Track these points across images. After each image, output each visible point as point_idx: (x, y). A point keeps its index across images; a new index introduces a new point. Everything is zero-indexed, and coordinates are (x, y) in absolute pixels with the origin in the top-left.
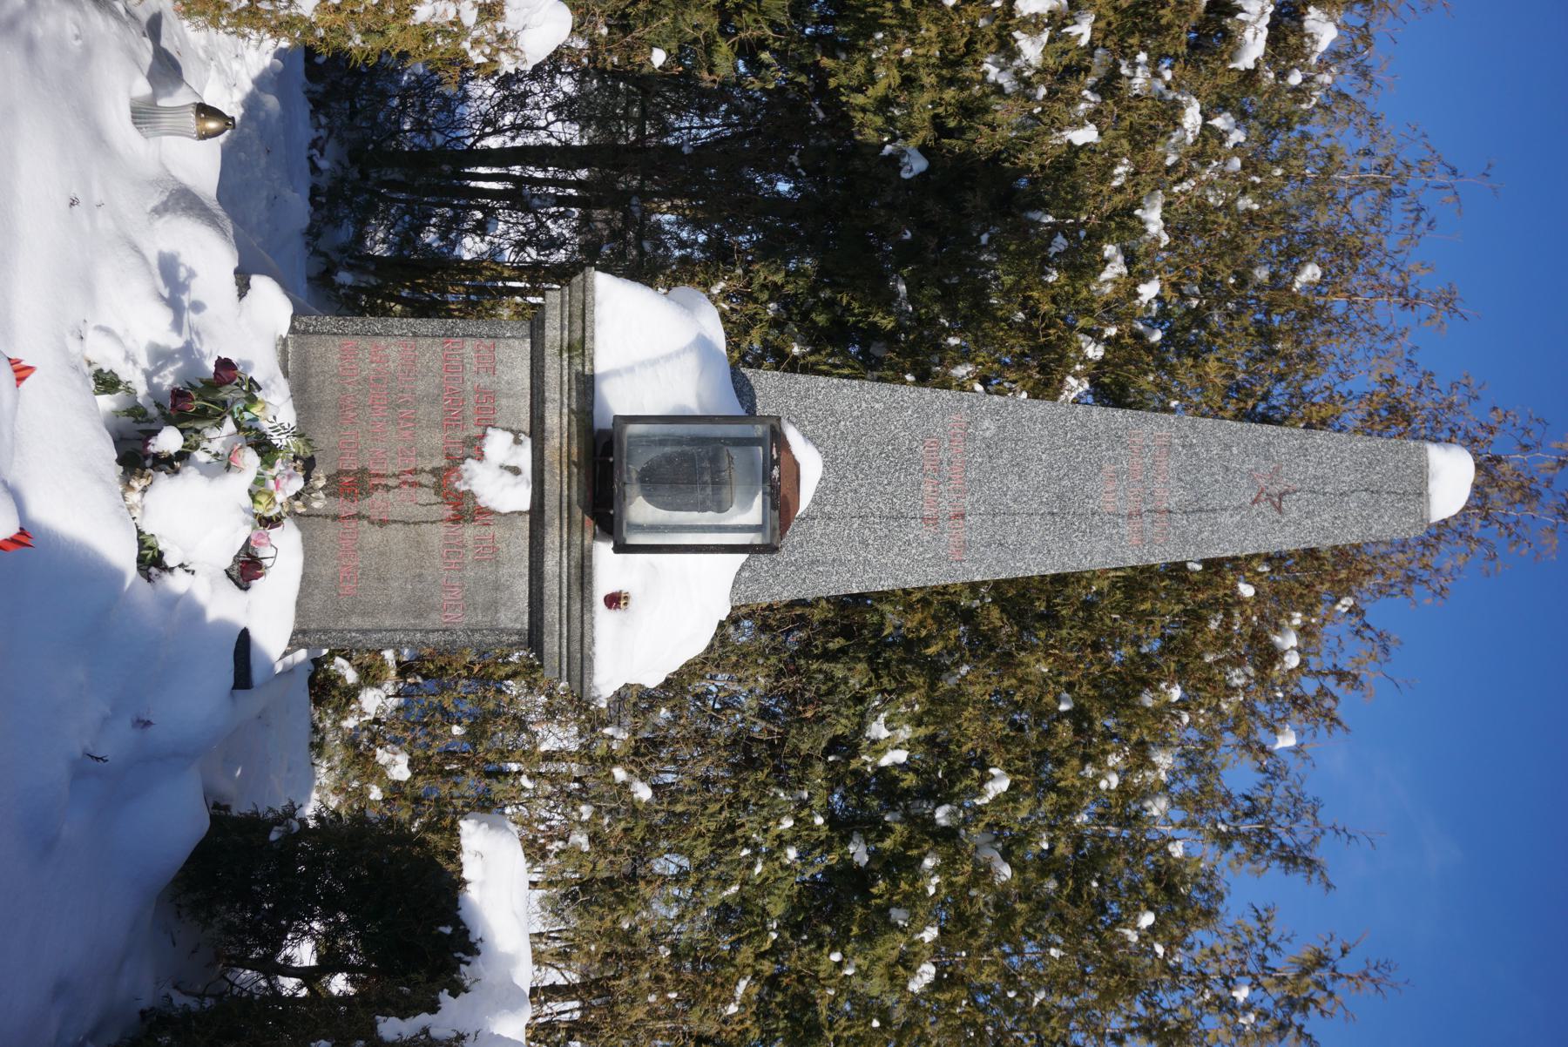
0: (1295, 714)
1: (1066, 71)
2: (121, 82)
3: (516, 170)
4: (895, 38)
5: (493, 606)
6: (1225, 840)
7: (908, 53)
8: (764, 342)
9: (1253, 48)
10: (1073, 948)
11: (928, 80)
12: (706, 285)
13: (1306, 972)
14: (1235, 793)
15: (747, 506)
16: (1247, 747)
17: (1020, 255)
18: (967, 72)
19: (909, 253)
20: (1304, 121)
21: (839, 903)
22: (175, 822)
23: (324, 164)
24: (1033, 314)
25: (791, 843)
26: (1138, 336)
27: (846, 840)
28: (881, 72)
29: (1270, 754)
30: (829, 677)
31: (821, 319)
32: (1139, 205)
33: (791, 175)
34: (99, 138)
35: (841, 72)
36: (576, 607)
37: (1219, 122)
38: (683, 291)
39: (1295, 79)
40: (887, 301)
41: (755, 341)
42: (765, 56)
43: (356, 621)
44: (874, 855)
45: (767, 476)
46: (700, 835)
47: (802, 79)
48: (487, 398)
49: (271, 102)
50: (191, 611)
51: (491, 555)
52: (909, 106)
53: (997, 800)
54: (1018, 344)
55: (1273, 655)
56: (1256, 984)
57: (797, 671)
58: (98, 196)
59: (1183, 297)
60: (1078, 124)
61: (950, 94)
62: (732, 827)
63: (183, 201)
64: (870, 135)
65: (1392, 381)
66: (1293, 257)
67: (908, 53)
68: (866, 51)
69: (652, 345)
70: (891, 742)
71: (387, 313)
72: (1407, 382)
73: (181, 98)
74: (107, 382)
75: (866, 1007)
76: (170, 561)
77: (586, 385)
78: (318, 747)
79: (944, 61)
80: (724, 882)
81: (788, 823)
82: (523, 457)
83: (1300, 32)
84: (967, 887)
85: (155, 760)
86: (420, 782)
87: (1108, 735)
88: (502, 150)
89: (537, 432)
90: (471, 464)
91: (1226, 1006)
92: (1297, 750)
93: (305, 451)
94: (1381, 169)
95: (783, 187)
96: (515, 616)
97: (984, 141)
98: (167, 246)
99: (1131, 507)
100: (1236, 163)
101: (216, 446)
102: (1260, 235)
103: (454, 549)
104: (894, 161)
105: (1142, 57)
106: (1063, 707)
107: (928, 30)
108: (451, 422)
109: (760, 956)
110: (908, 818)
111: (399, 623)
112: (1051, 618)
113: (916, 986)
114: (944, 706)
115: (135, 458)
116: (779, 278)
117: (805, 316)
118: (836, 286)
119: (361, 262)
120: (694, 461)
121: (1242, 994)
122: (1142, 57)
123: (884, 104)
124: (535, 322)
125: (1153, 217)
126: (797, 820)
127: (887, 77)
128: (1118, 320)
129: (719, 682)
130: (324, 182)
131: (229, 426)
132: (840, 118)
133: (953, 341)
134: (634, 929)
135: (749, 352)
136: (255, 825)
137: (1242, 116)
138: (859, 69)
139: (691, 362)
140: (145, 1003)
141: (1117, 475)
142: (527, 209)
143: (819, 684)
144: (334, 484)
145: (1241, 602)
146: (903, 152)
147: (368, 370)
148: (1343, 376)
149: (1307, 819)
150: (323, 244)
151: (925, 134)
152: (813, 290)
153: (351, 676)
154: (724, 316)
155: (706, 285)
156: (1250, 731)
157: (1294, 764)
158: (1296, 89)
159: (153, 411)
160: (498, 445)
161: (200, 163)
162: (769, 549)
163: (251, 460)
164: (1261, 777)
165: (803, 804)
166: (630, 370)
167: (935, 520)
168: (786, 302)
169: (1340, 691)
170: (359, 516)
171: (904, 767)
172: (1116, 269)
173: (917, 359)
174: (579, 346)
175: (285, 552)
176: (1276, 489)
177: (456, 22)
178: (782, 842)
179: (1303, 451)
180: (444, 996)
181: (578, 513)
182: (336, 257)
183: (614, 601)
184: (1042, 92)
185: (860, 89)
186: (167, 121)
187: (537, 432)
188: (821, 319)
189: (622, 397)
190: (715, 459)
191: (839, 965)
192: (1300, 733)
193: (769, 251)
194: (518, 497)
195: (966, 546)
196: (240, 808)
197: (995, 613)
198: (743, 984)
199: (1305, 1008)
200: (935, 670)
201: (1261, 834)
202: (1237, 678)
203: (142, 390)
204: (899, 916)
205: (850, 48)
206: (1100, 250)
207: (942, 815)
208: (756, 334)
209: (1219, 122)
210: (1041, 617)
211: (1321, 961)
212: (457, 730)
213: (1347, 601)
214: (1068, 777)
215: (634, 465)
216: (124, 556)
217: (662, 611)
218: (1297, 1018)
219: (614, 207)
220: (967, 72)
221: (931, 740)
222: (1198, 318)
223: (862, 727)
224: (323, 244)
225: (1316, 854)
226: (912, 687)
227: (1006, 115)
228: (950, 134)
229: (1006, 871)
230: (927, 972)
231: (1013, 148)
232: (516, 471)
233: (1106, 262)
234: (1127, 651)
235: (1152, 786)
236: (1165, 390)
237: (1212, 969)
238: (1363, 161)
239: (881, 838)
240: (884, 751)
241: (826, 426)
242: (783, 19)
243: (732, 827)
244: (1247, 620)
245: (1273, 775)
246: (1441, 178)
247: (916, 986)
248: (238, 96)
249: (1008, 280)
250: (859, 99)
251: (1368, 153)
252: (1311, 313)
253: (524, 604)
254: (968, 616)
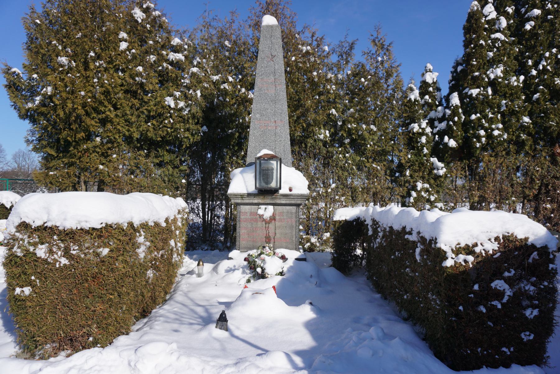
0: (321, 46)
1: (186, 97)
2: (194, 279)
3: (207, 210)
4: (179, 132)
5: (291, 213)
6: (347, 62)
7: (182, 130)
8: (241, 160)
9: (180, 56)
10: (369, 95)
11: (188, 126)
12: (230, 172)
13: (376, 45)
14: (337, 59)
15: (273, 164)
16: (327, 57)
17: (223, 107)
18: (186, 118)
19: (223, 130)
20: (195, 45)
21: (358, 145)
22: (332, 273)
23: (206, 248)
24: (235, 103)
25: (345, 155)
26: (240, 81)
27: (344, 144)
28: (186, 135)
29: (329, 52)
30: (310, 147)
31: (236, 148)
32: (213, 81)
33: (206, 154)
34: (205, 282)
35: (186, 144)
36: (292, 197)
37: (195, 63)
38: (231, 176)
39: (186, 47)
40: (233, 134)
41: (241, 162)
42: (183, 159)
43: (294, 239)
44: (347, 137)
45: (267, 160)
46: (343, 174)
47: (188, 152)
48: (251, 214)
49: (195, 256)
50: (291, 269)
51: (281, 214)
52: (193, 130)
53: (337, 112)
54: (242, 108)
55: (307, 52)
56: (379, 55)
57: (309, 154)
58: (215, 282)
59: (232, 71)
60: (196, 94)
61: (190, 121)
62: (341, 167)
63: (215, 269)
64: (199, 138)
65: (250, 26)
66: (223, 47)
67: (182, 130)
68: (182, 138)
69: (241, 182)
70: (324, 134)
71: (236, 237)
72: (250, 22)
73: (196, 270)
74: (248, 281)
75: (380, 140)
76: (281, 271)
77: (249, 195)
78: (323, 251)
79: (184, 122)
80: (352, 169)
81: (341, 156)
82: (263, 207)
83: (176, 46)
84: (355, 118)
85: (319, 274)
86: (330, 231)
87: (324, 88)
88: (202, 212)
89: (258, 204)
90: (264, 217)
91: (382, 62)
92: (328, 46)
93: (261, 247)
94: (205, 27)
95: (209, 155)
96: (293, 209)
97: (200, 114)
98: (223, 271)
99: (274, 87)
100: (204, 60)
101: (260, 262)
102: (219, 54)
103: (280, 220)
104: (204, 133)
105: (182, 81)
106: (317, 98)
107: (178, 126)
108: (256, 221)
109: (368, 162)
110: (340, 131)
111: (294, 231)
112: (299, 100)
113: (375, 129)
114: (316, 123)
115: (263, 276)
116: (228, 157)
117: (236, 151)
118: (230, 145)
119: (226, 241)
120: (264, 174)
121: (380, 59)
122: (182, 81)
123: (192, 135)
124: (237, 204)
125: (215, 78)
126: (340, 154)
127: (187, 134)
128: (237, 85)
129: (312, 170)
130: (210, 248)
131: (256, 260)
132: (196, 144)
133: (241, 121)
134: (362, 188)
135: (243, 163)
136: (334, 259)
137: (194, 58)
138: (185, 140)
139: (245, 175)
140: (366, 279)
141: (267, 90)
142: (215, 208)
143: (312, 149)
144: (269, 242)
145: (296, 60)
146: (202, 131)
147: (246, 236)
148: (248, 36)
149: (343, 44)
150: (222, 248)
151: (199, 126)
152: (230, 149)
153: (309, 244)
154: (236, 168)
155: (230, 172)
156: (324, 57)
157: (331, 47)
158: (188, 46)
159: (254, 273)
160: (261, 212)
161: (208, 267)
162: (280, 160)
163: (262, 256)
164: (334, 54)
165: (337, 152)
166: (246, 186)
167: (276, 127)
168: (233, 155)
169: (316, 36)
170: (274, 238)
171: (330, 131)
172: (226, 86)
173: (244, 128)
174: (242, 196)
175: (281, 251)
176: (271, 56)
177: (181, 218)
178: (345, 157)
179: (263, 51)
180: (366, 223)
181: (274, 197)
182: (224, 246)
183: (290, 190)
184: (190, 102)
185: (190, 140)
186: (200, 272)
187: (258, 204)
188: (236, 148)
189: (252, 188)
190: (263, 170)
191: (370, 145)
192: (325, 45)
193: (222, 158)
194: (271, 209)
195: (281, 121)
196: (331, 263)
197: (298, 112)
198: (374, 165)
199: (384, 45)
200: (309, 125)
201: (346, 54)
202: (312, 59)
203: (250, 275)
204: (360, 133)
205: (181, 142)
206: (222, 89)
207: (340, 123)
208: (239, 162)
209: (195, 63)
210: (299, 102)
211: (374, 41)
212: (320, 223)
213: (297, 35)
214: (332, 97)
215: (264, 185)
216: (280, 278)
217: (293, 181)
218: (385, 47)
219: (214, 190)
220: (186, 118)
221: (324, 126)
222: (236, 67)
223: (321, 140)
224: (222, 248)
225: (351, 42)
226: (313, 130)
227: (195, 109)
228: (198, 121)
229: (352, 110)
230: (372, 127)
231: (201, 108)
232: (266, 208)
233: (225, 88)
234: (306, 84)
235: (334, 77)
236: (251, 75)
237: (375, 65)
238: (203, 31)
239: (344, 136)
240: (326, 136)
241: (257, 149)
242: (175, 155)
243: (341, 167)
244: (300, 58)
245: (334, 51)
246: (206, 14)
247: (375, 129)
248: (194, 262)
249: (228, 109)
250: (192, 140)
251: (201, 30)
252: (235, 43)
253: (291, 207)
254: (298, 118)
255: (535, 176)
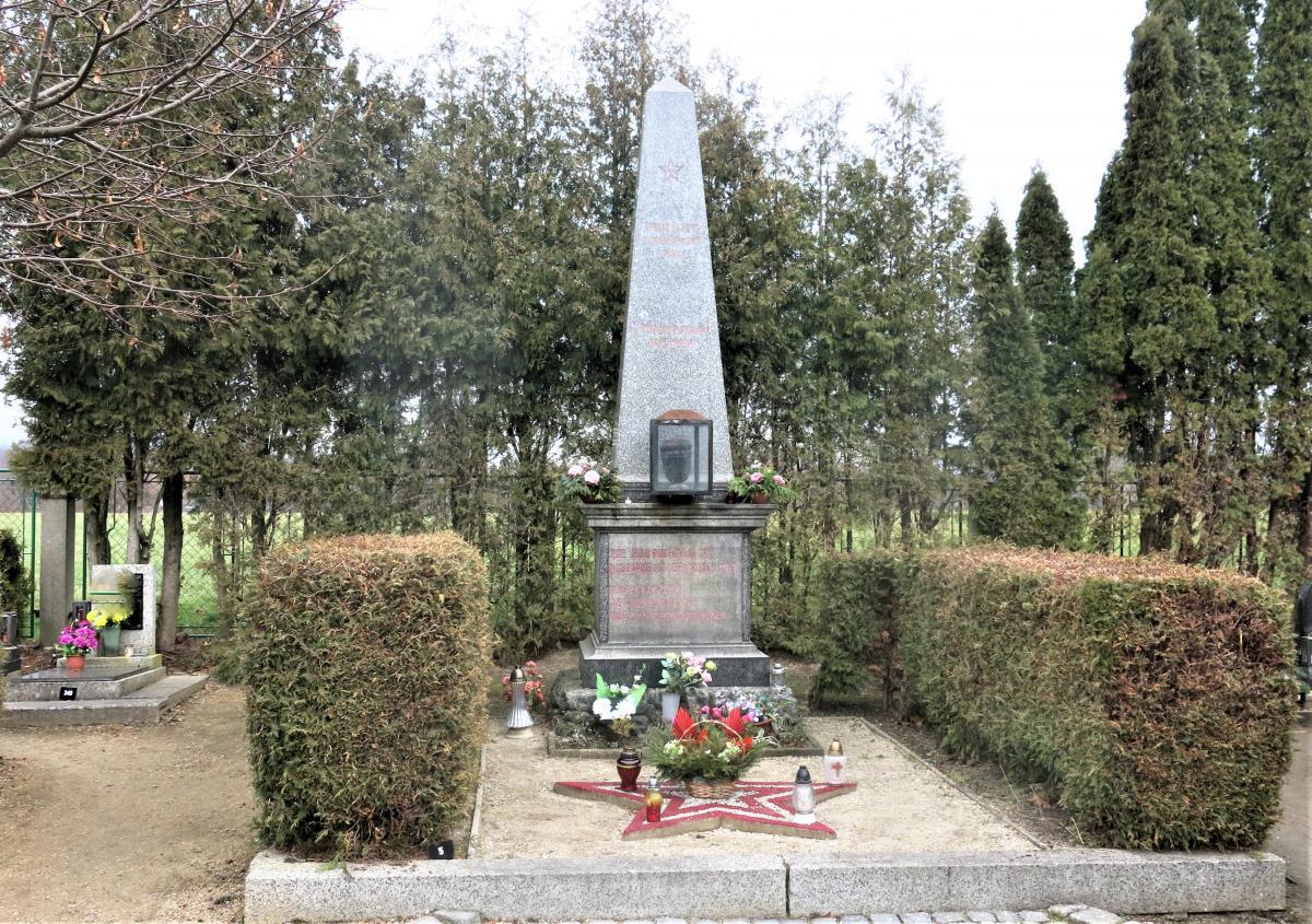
5: (732, 550)
43: (738, 611)
111: (739, 592)
147: (624, 607)
255: (1298, 450)
